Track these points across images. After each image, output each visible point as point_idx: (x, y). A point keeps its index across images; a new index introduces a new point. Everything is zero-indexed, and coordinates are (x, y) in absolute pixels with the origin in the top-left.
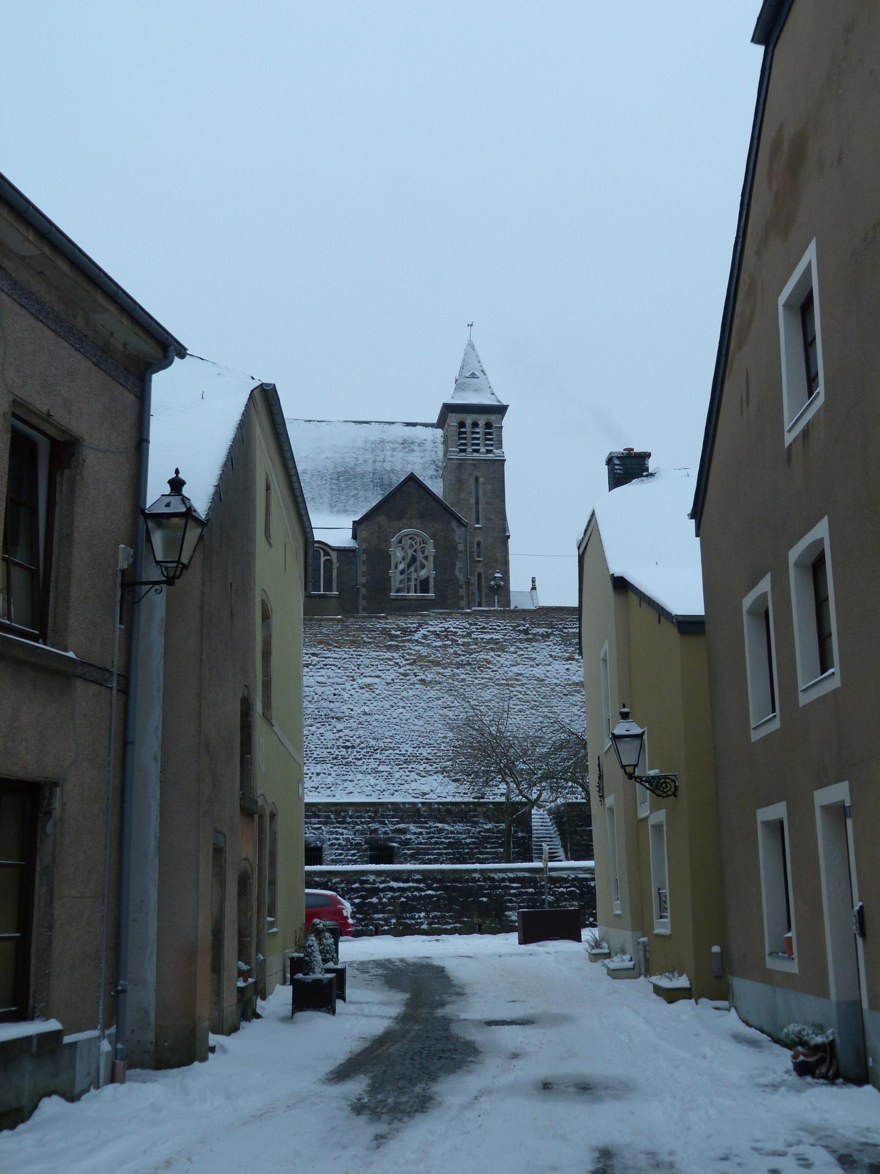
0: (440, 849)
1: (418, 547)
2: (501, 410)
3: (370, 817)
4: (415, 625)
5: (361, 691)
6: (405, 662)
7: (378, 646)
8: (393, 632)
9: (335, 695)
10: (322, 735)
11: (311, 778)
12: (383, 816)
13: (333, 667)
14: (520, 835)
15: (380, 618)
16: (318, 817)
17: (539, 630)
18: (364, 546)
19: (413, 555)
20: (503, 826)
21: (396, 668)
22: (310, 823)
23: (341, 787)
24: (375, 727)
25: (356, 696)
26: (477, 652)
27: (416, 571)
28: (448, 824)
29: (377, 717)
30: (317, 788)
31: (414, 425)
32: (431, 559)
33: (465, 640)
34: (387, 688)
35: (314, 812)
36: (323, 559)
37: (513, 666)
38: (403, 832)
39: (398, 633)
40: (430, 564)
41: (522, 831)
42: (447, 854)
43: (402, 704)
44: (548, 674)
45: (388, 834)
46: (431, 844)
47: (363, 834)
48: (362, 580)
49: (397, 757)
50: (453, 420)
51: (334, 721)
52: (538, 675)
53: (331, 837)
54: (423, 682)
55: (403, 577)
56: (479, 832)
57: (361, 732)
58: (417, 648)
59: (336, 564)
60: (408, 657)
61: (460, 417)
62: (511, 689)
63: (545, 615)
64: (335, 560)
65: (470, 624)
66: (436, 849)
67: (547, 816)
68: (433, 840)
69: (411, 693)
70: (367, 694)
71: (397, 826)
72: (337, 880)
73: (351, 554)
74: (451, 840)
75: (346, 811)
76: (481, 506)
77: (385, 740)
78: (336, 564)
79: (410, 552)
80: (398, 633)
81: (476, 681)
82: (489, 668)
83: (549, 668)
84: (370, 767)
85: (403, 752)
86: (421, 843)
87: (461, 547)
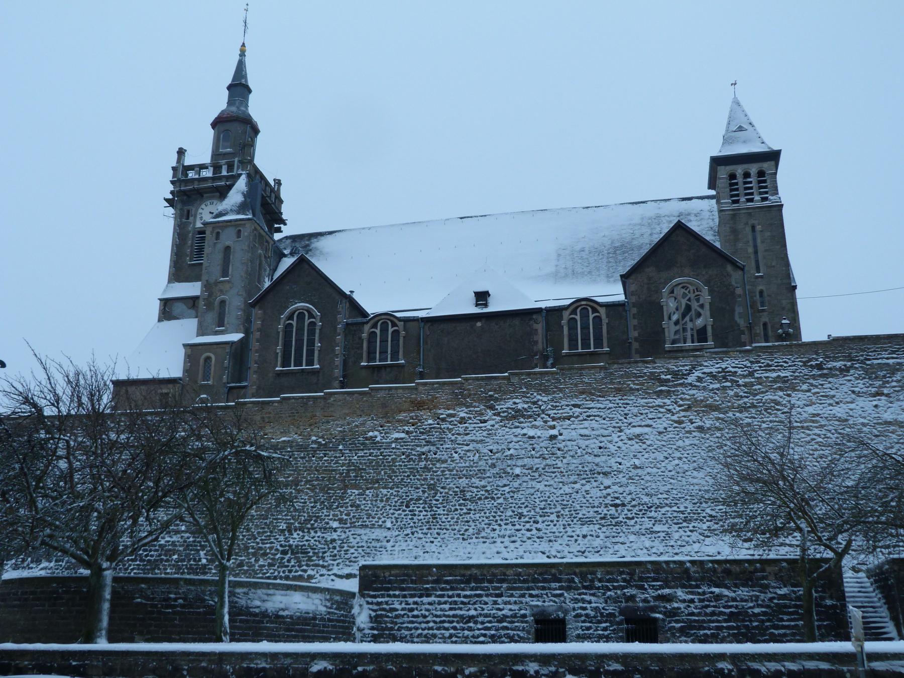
0: (718, 621)
1: (692, 296)
2: (773, 156)
3: (624, 580)
4: (687, 368)
5: (630, 442)
6: (678, 409)
7: (647, 393)
8: (663, 377)
9: (600, 448)
10: (587, 492)
11: (576, 541)
12: (641, 579)
13: (597, 418)
14: (829, 602)
15: (647, 362)
16: (559, 581)
17: (835, 364)
18: (633, 299)
19: (687, 304)
20: (801, 591)
21: (669, 416)
22: (549, 589)
23: (611, 551)
24: (647, 481)
25: (624, 448)
26: (763, 393)
27: (691, 320)
28: (728, 588)
29: (649, 470)
30: (583, 552)
31: (690, 199)
32: (707, 306)
33: (747, 380)
34: (659, 438)
35: (554, 575)
36: (591, 317)
37: (807, 406)
38: (668, 599)
39: (669, 377)
40: (706, 312)
41: (831, 598)
42: (728, 628)
43: (677, 454)
44: (851, 413)
45: (649, 602)
46: (706, 614)
47: (615, 602)
48: (634, 334)
49: (675, 514)
50: (723, 172)
51: (600, 478)
52: (839, 415)
53: (576, 606)
54: (700, 429)
55: (677, 327)
56: (771, 599)
57: (632, 488)
58: (692, 392)
59: (605, 321)
60: (681, 402)
61: (730, 169)
62: (808, 432)
63: (841, 346)
64: (604, 316)
65: (752, 362)
66: (713, 622)
67: (866, 580)
68: (709, 610)
69: (687, 442)
70: (637, 446)
71: (659, 592)
72: (472, 669)
73: (620, 309)
74: (733, 610)
75: (594, 573)
76: (760, 255)
77: (660, 496)
78: (605, 321)
79: (684, 302)
80: (669, 377)
81: (764, 425)
82: (778, 410)
83: (852, 406)
84: (644, 527)
85: (682, 509)
86: (692, 614)
87: (739, 291)
